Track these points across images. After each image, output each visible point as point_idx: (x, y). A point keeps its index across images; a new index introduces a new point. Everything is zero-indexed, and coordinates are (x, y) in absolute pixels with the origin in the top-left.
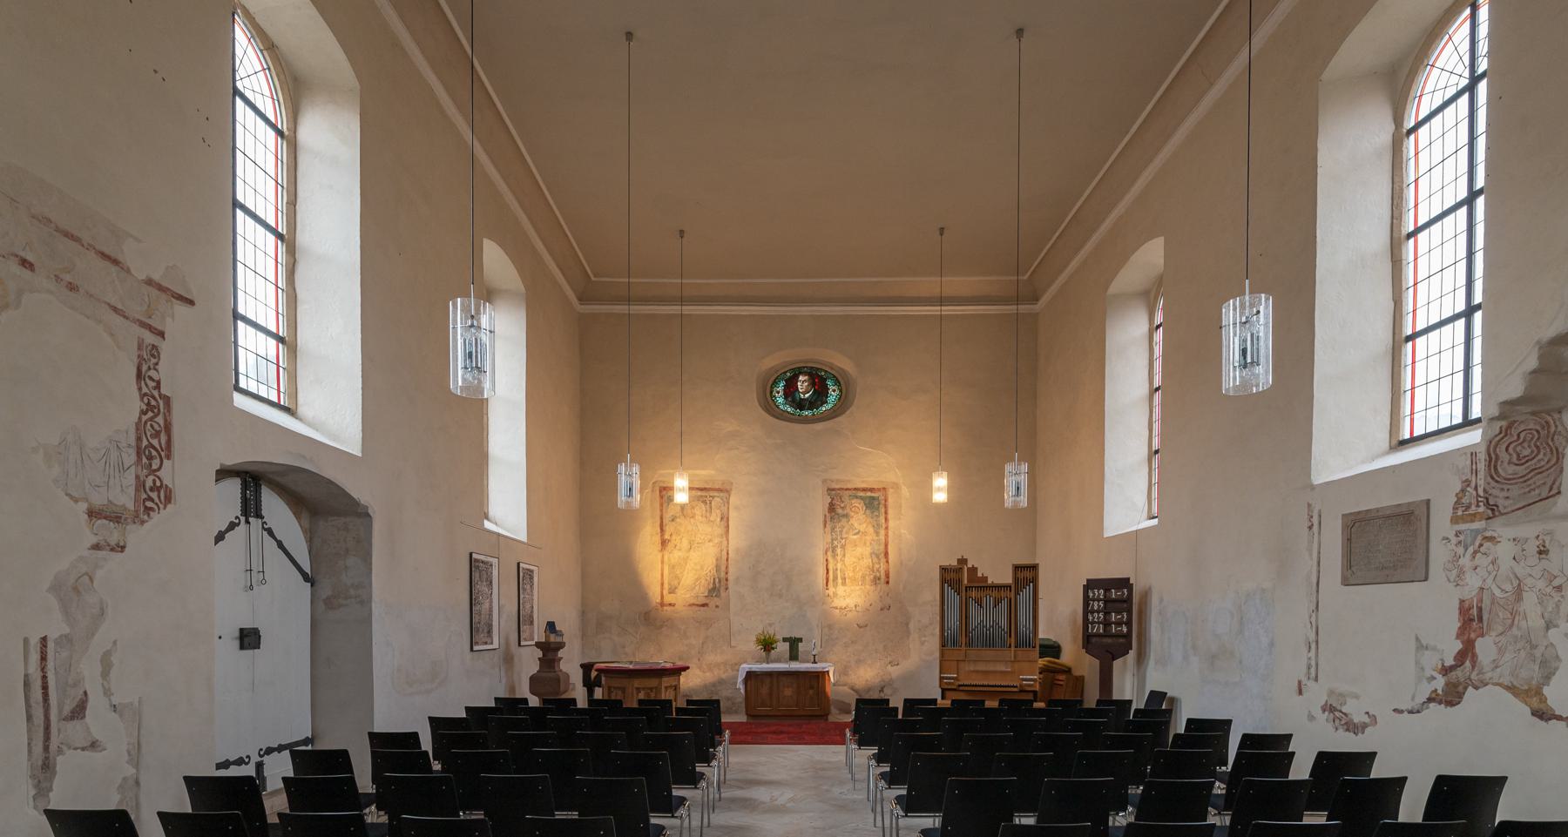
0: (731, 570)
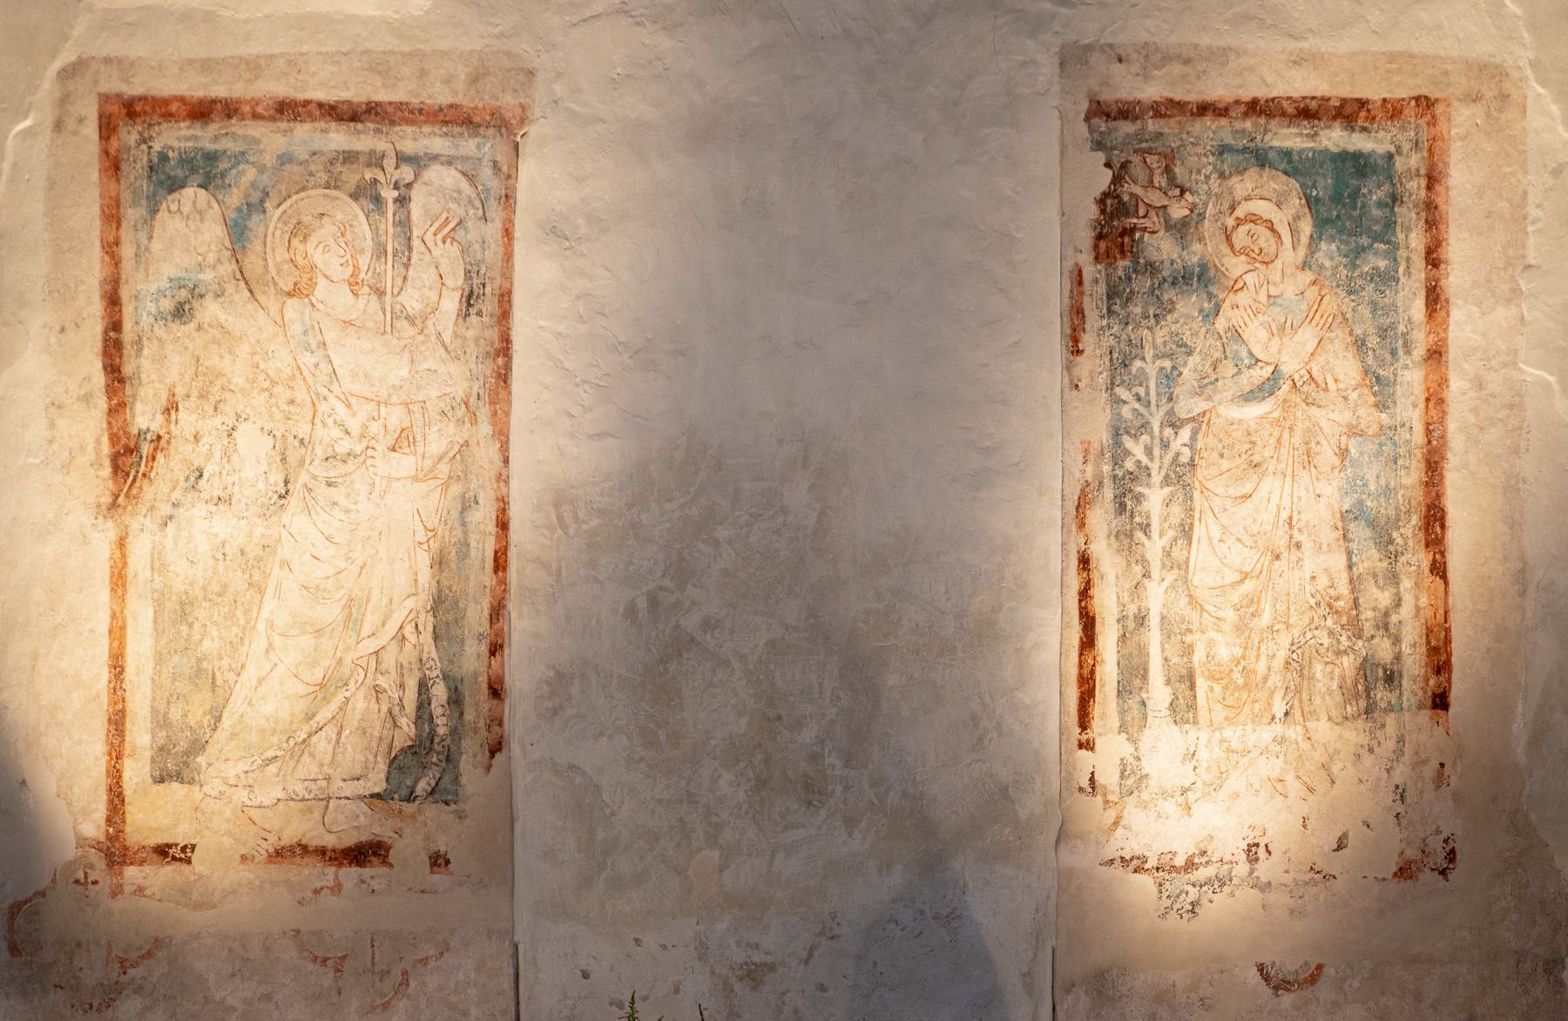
0: (521, 625)
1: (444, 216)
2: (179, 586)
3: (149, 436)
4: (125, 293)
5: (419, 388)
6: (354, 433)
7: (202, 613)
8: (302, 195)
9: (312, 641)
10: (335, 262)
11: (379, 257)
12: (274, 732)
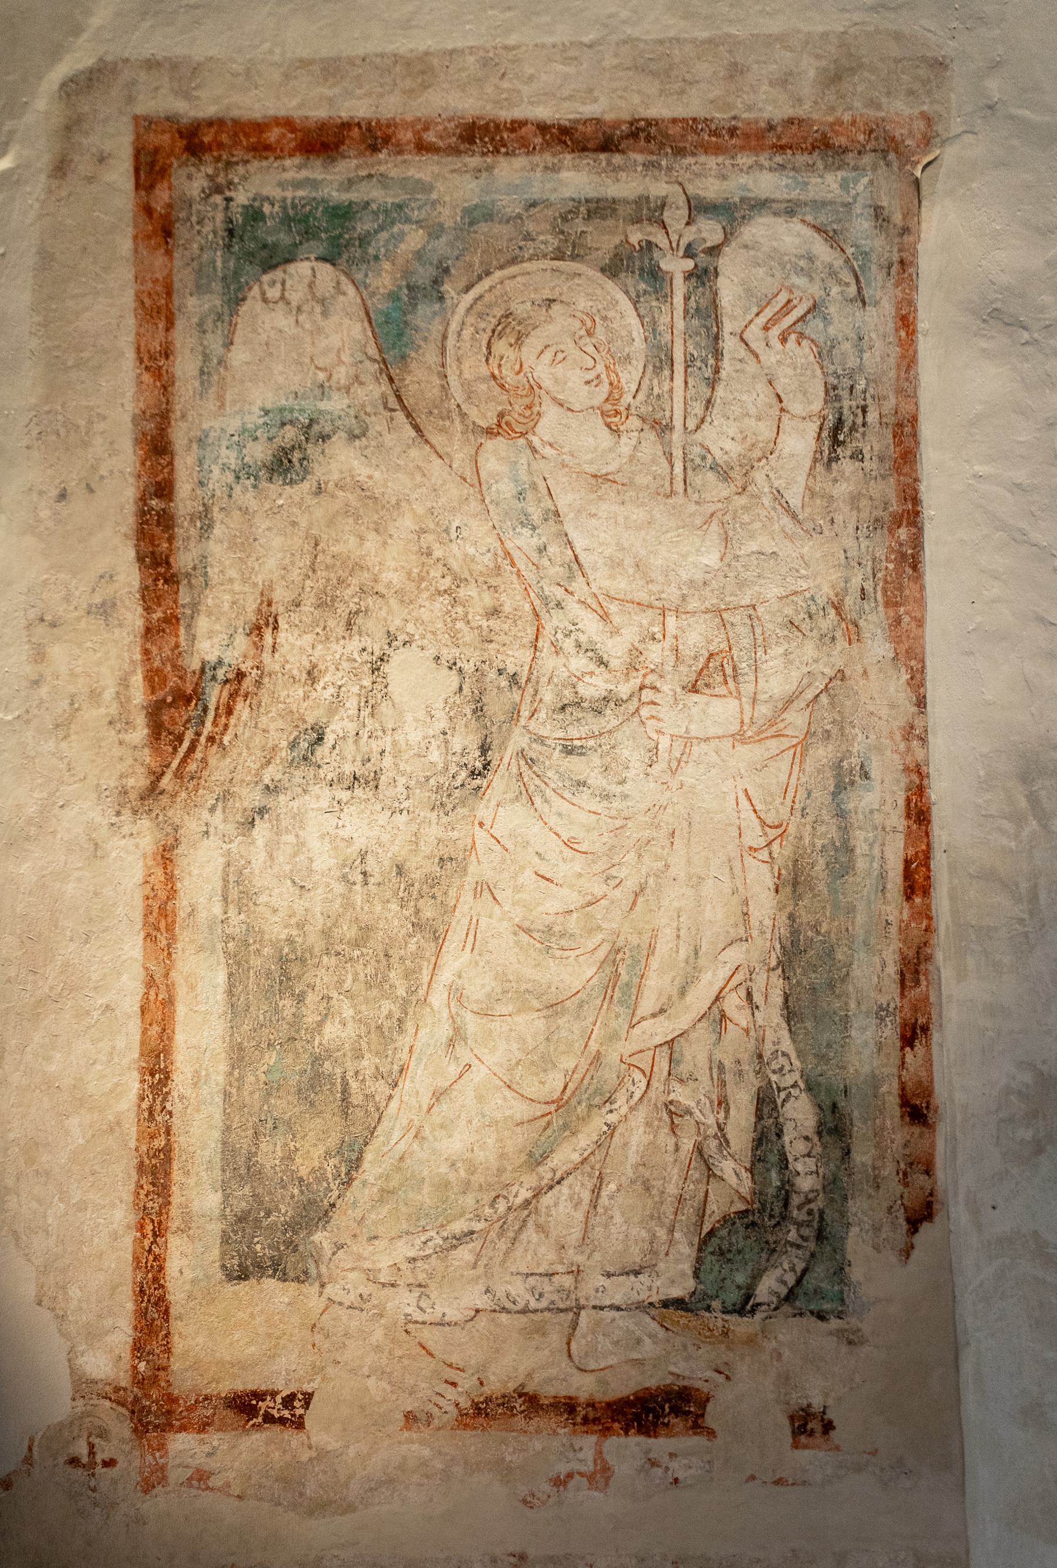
0: (961, 991)
1: (782, 298)
2: (277, 930)
3: (220, 673)
4: (179, 435)
5: (742, 584)
6: (614, 663)
7: (322, 977)
8: (513, 270)
9: (541, 1024)
10: (575, 378)
11: (658, 370)
12: (466, 1187)
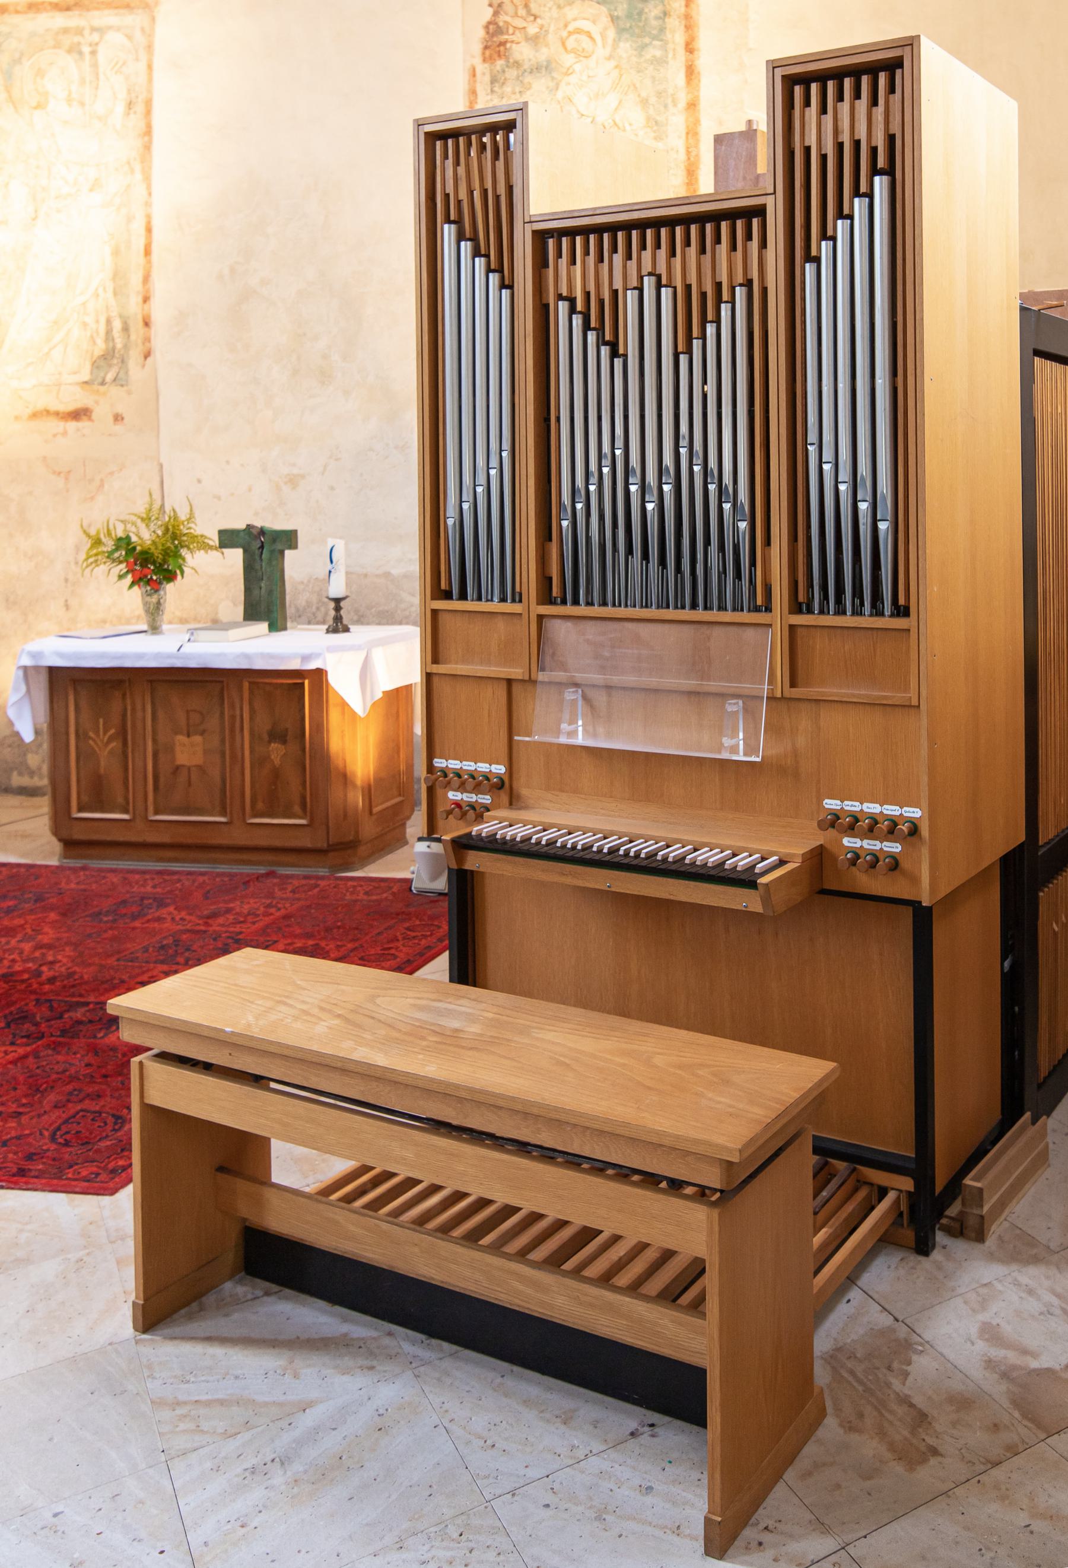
0: (160, 286)
